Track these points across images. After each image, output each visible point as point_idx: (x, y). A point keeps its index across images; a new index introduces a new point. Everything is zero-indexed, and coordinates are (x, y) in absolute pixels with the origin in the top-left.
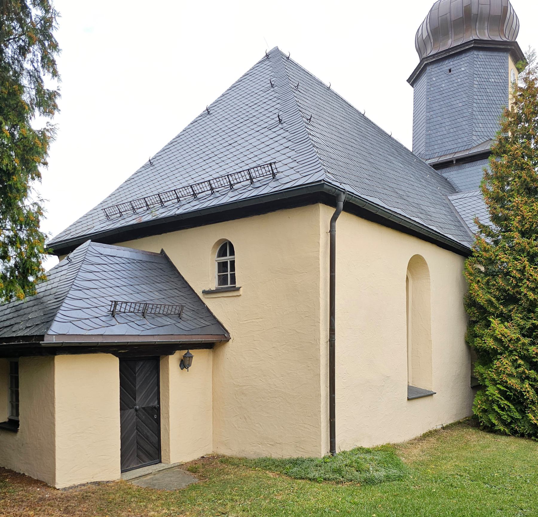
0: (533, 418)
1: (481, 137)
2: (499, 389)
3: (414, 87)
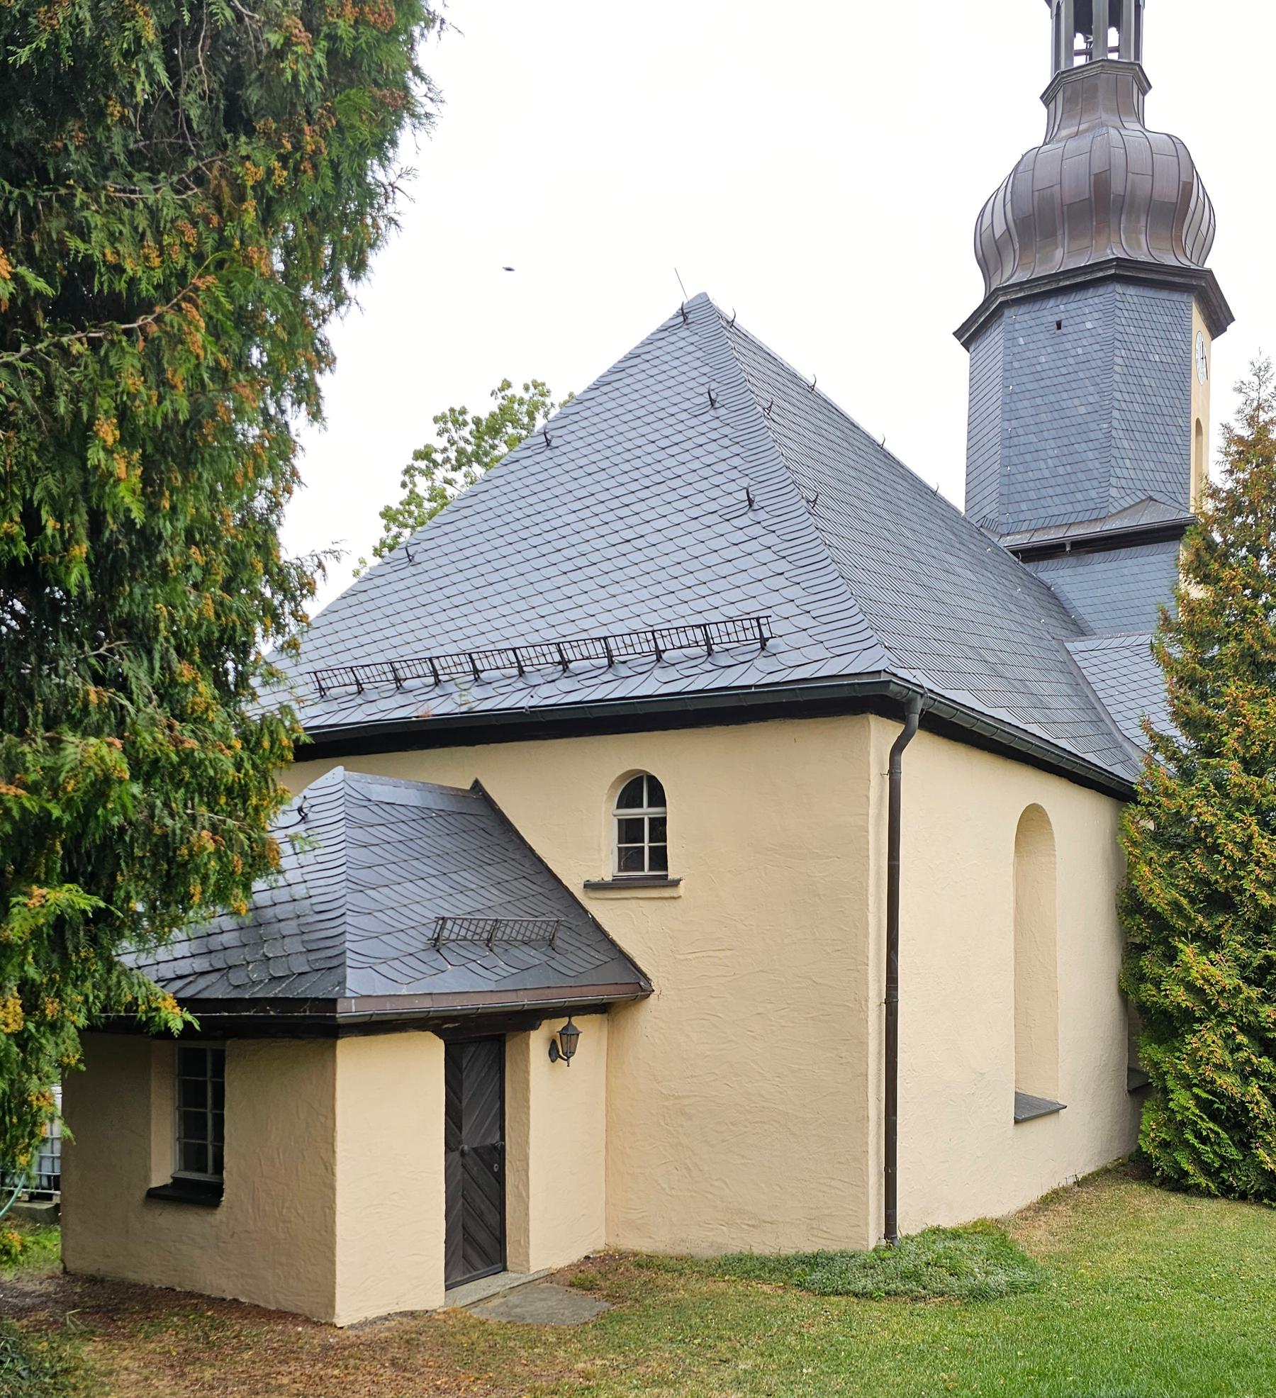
0: (1268, 1159)
1: (1129, 492)
2: (1197, 1097)
3: (971, 349)
